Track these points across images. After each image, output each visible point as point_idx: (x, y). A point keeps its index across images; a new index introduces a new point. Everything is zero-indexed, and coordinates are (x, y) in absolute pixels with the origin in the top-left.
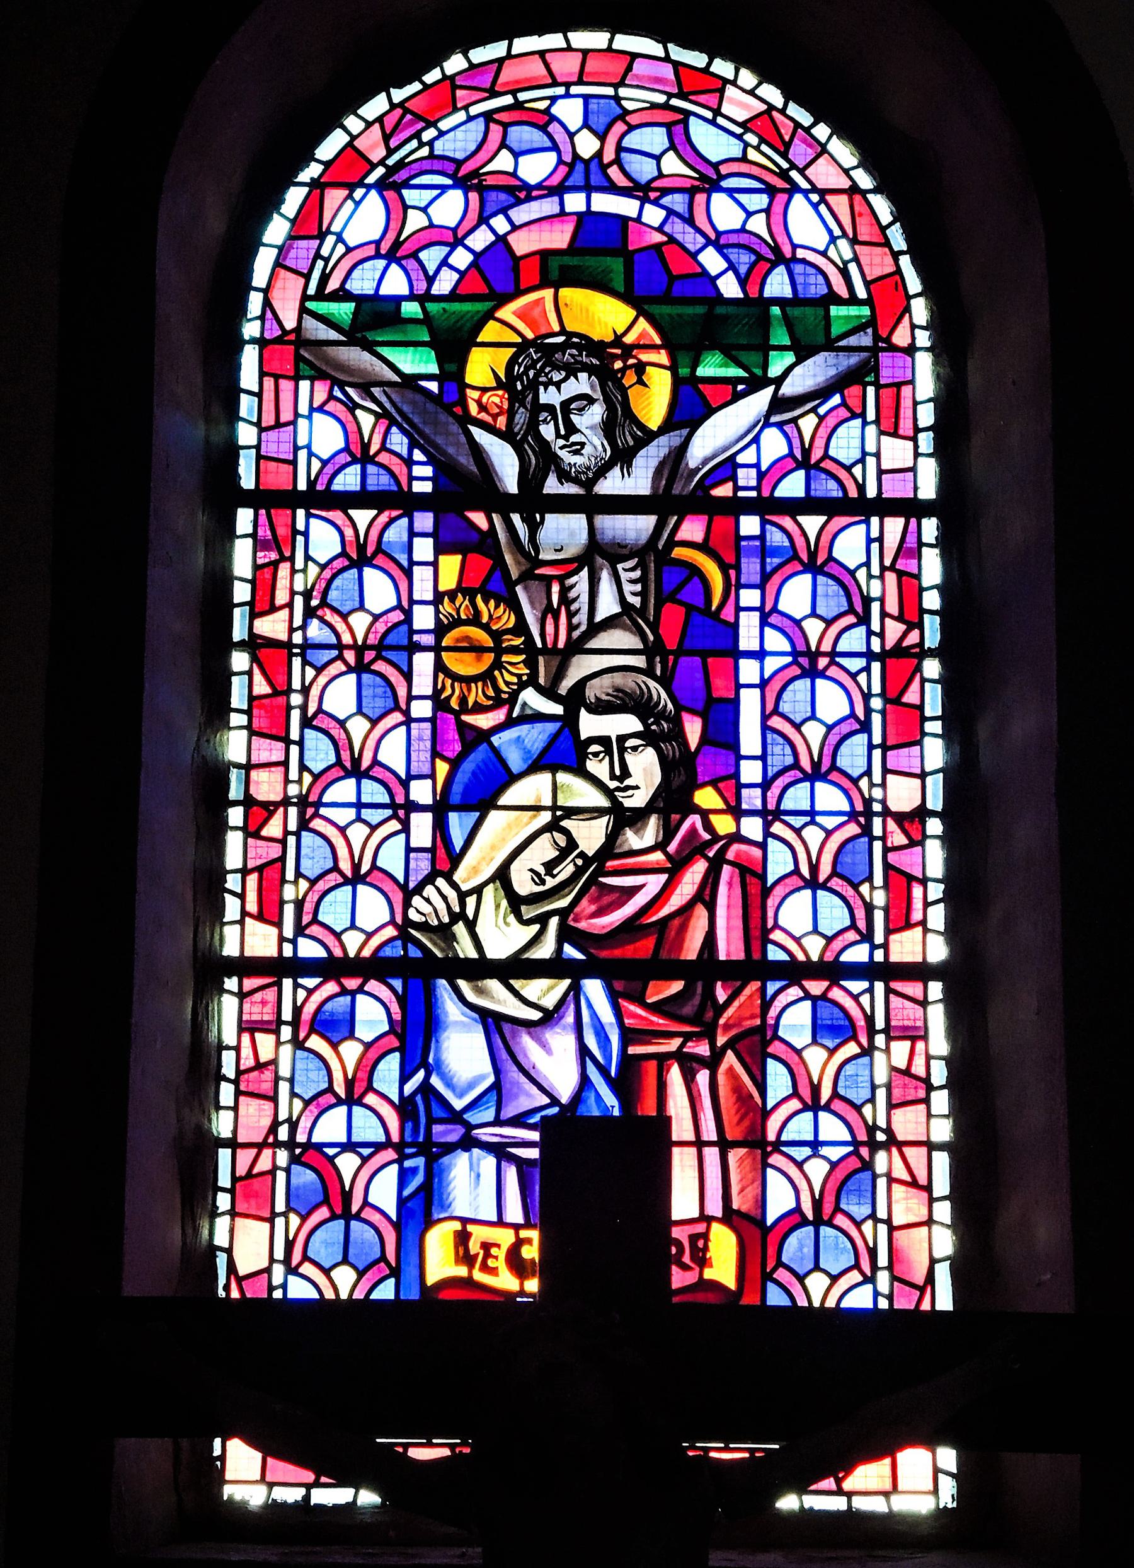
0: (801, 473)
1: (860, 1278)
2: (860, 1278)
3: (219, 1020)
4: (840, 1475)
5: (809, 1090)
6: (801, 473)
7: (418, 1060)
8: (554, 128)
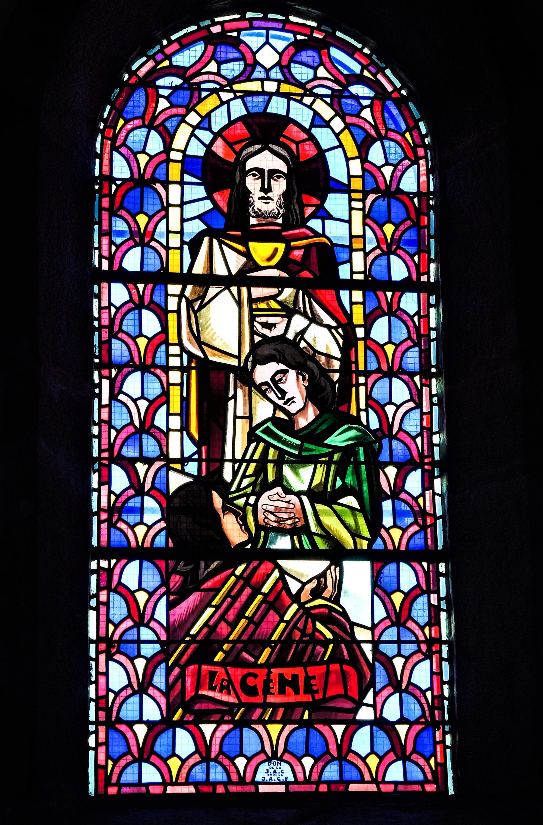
0: (139, 249)
1: (265, 758)
2: (265, 758)
3: (323, 472)
4: (308, 93)
5: (335, 747)
6: (139, 249)
7: (390, 727)
8: (242, 47)
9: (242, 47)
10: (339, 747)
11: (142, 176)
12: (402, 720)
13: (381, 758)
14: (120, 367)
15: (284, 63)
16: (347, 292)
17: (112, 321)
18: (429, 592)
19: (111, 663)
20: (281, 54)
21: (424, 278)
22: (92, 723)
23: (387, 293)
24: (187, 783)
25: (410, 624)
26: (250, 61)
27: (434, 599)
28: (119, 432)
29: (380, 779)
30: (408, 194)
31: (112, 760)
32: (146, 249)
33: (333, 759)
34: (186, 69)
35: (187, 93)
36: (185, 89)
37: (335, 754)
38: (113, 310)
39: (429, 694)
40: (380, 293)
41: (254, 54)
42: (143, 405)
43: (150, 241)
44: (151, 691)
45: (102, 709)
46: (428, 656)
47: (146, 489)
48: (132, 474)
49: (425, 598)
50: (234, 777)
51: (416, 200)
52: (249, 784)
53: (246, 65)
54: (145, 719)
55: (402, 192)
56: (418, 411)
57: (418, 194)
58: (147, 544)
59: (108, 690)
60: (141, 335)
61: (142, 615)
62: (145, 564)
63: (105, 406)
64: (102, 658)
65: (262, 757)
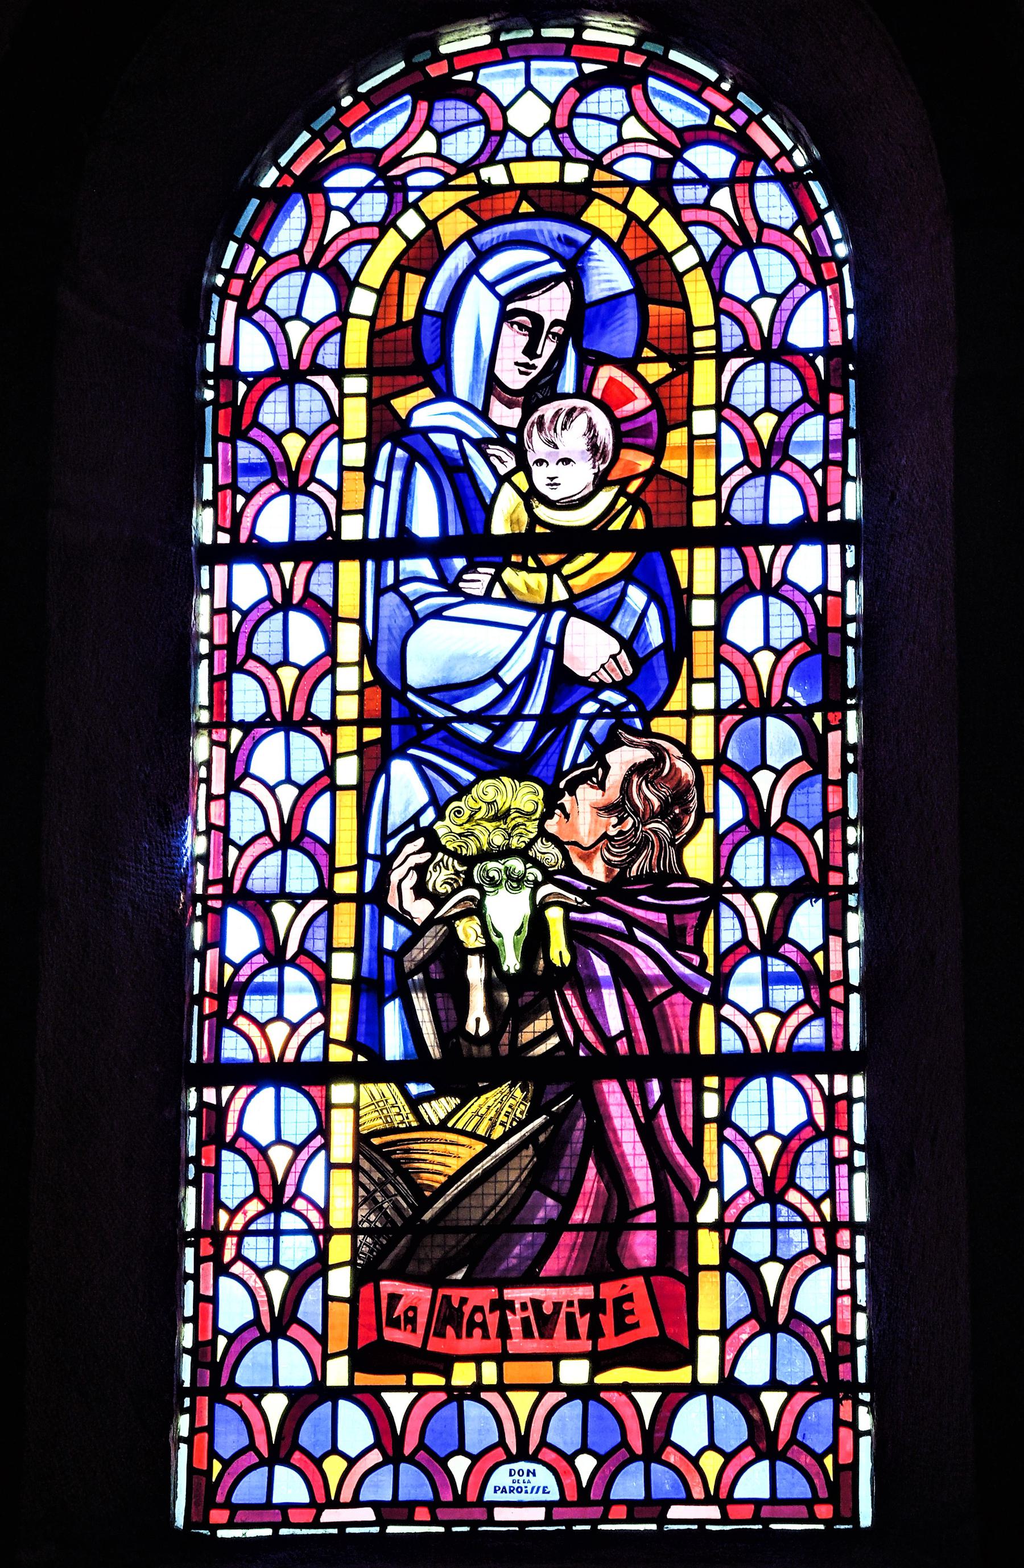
8: (483, 100)
9: (483, 100)
10: (647, 1435)
11: (294, 363)
12: (774, 1384)
13: (728, 1457)
14: (246, 727)
15: (560, 122)
16: (685, 552)
17: (233, 637)
18: (830, 1133)
19: (223, 1281)
20: (553, 107)
21: (834, 516)
22: (187, 1392)
23: (762, 548)
24: (356, 1503)
25: (793, 1196)
26: (497, 125)
27: (841, 1146)
28: (242, 849)
29: (723, 1495)
30: (804, 352)
31: (220, 1459)
32: (300, 499)
33: (633, 1458)
34: (378, 152)
35: (382, 198)
36: (379, 190)
37: (638, 1449)
38: (236, 617)
39: (826, 1332)
40: (748, 551)
41: (504, 110)
42: (288, 795)
43: (308, 483)
44: (294, 1331)
45: (205, 1366)
46: (829, 1260)
47: (289, 954)
48: (266, 925)
49: (821, 1145)
50: (447, 1496)
51: (820, 361)
52: (472, 1505)
53: (489, 134)
54: (283, 1383)
55: (794, 350)
56: (819, 777)
57: (827, 351)
58: (290, 1056)
59: (217, 1331)
60: (286, 662)
61: (279, 1189)
62: (285, 1091)
63: (218, 797)
64: (208, 1269)
65: (499, 1454)
